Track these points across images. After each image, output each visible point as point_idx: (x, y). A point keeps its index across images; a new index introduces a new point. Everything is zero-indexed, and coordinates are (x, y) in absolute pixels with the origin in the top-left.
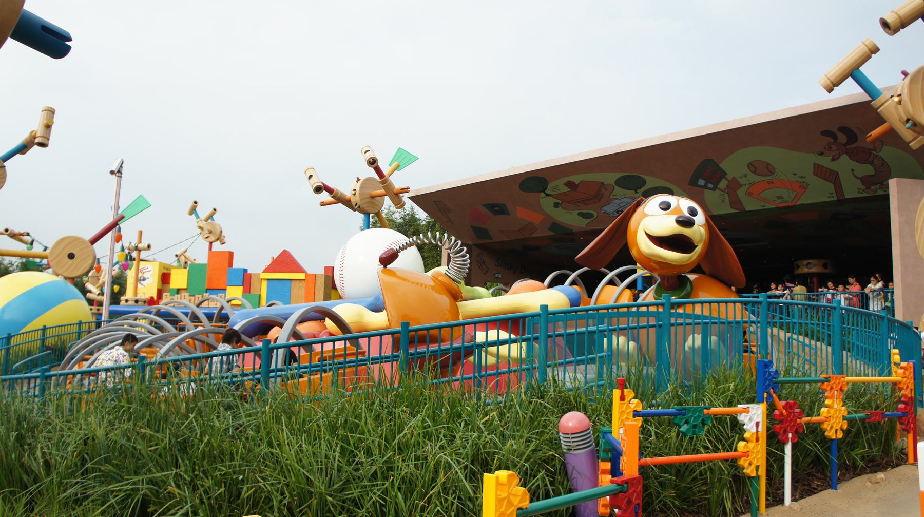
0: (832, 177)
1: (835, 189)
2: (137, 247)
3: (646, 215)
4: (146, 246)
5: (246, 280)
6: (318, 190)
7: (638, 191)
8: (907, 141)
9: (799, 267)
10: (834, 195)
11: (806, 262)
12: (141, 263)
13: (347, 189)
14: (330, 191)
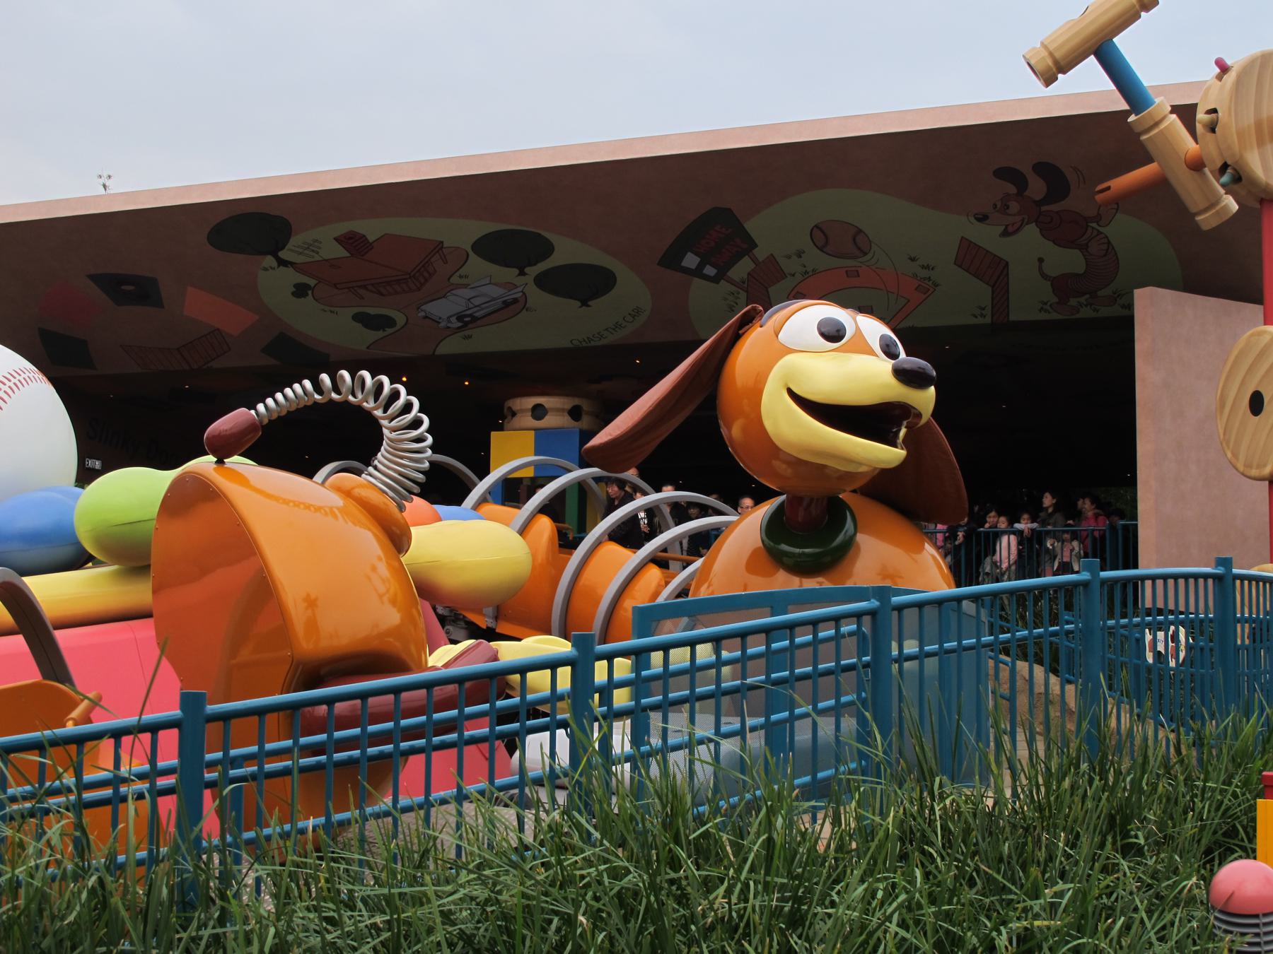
7: (527, 270)
8: (1193, 210)
10: (988, 312)
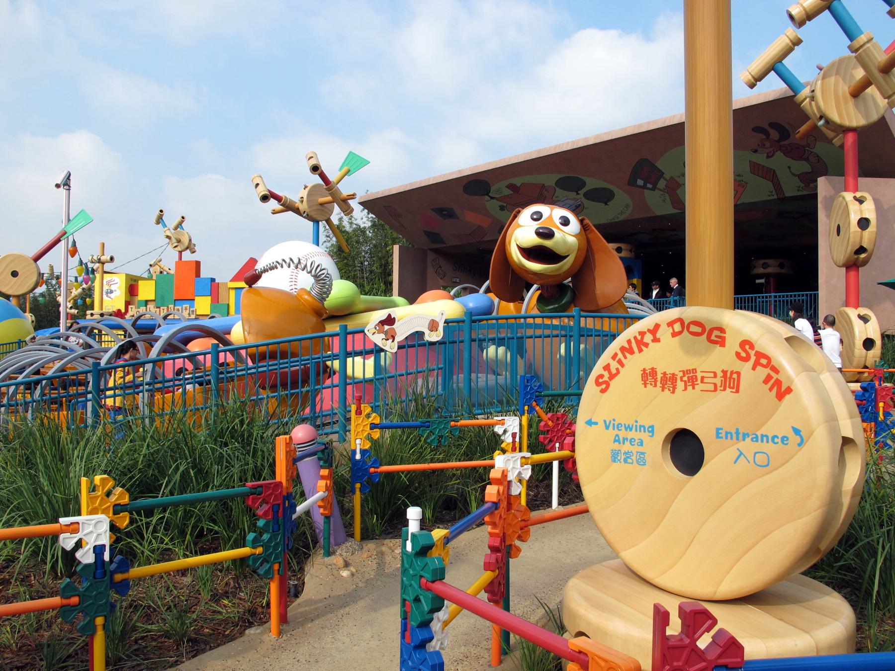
0: (770, 175)
1: (774, 187)
2: (100, 259)
3: (519, 226)
4: (109, 258)
5: (214, 289)
6: (265, 198)
7: (579, 192)
9: (755, 267)
10: (774, 193)
11: (762, 262)
12: (105, 275)
13: (296, 195)
14: (278, 199)
